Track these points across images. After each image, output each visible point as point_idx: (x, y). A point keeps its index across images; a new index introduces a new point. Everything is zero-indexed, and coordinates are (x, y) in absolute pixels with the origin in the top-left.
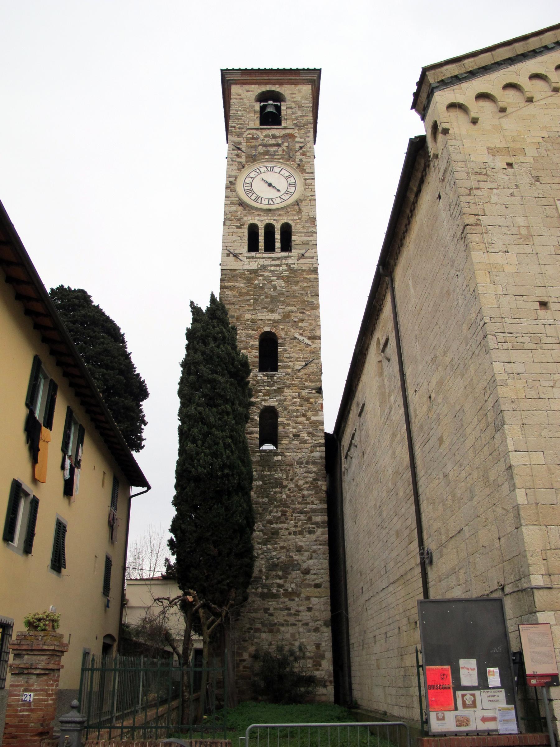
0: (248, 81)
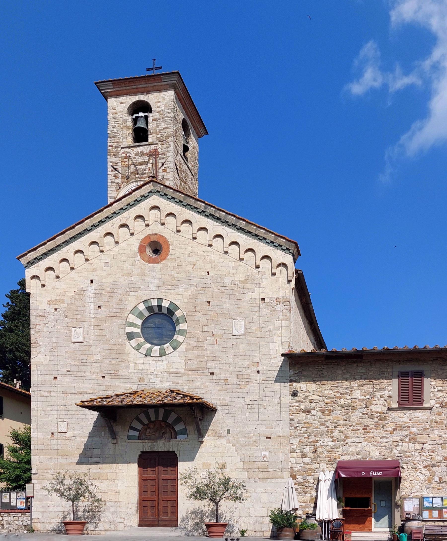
0: (120, 92)
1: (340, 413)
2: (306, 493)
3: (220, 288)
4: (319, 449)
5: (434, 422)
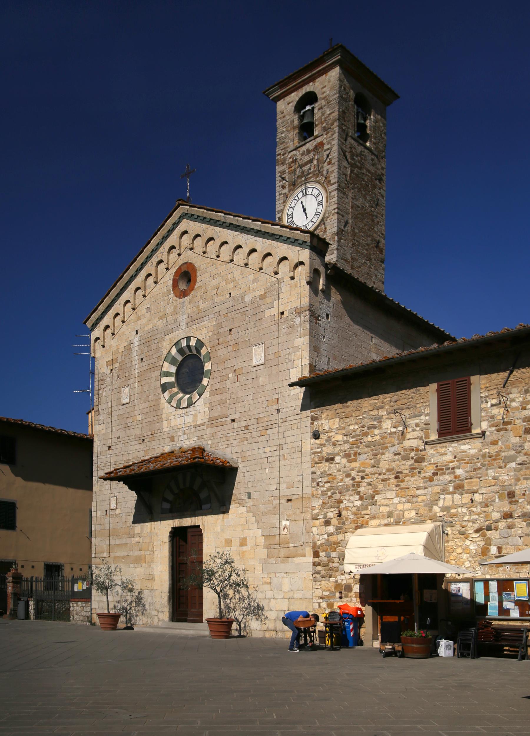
1: (368, 456)
2: (330, 577)
3: (242, 311)
4: (344, 513)
5: (487, 456)
